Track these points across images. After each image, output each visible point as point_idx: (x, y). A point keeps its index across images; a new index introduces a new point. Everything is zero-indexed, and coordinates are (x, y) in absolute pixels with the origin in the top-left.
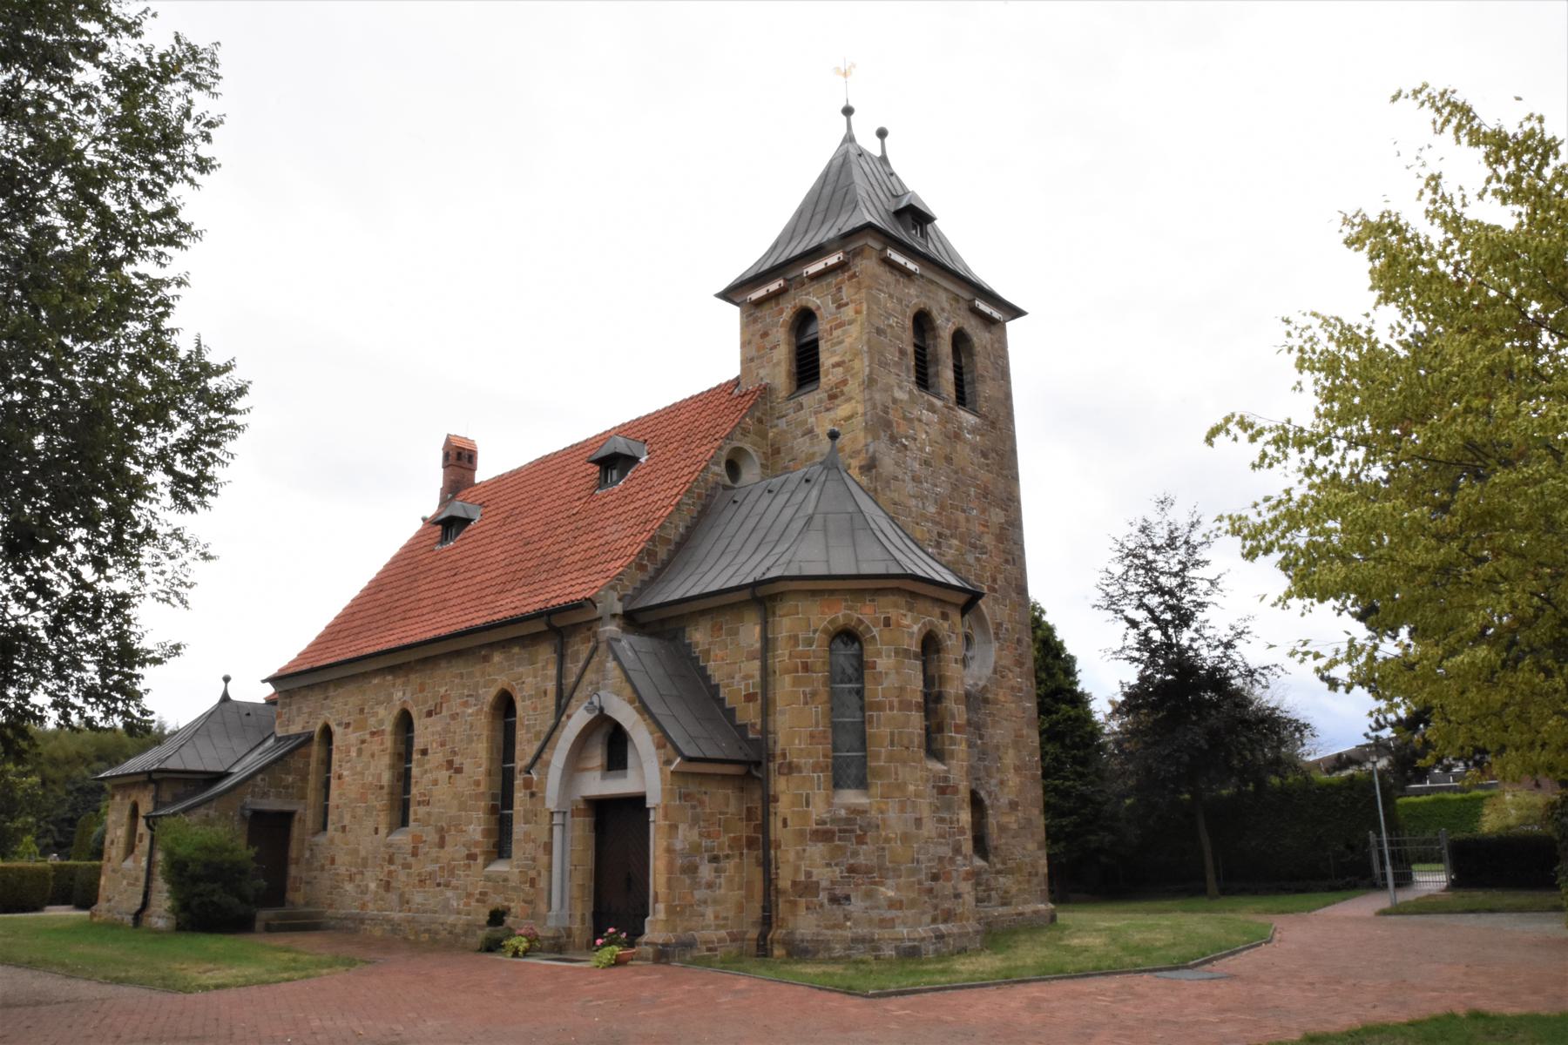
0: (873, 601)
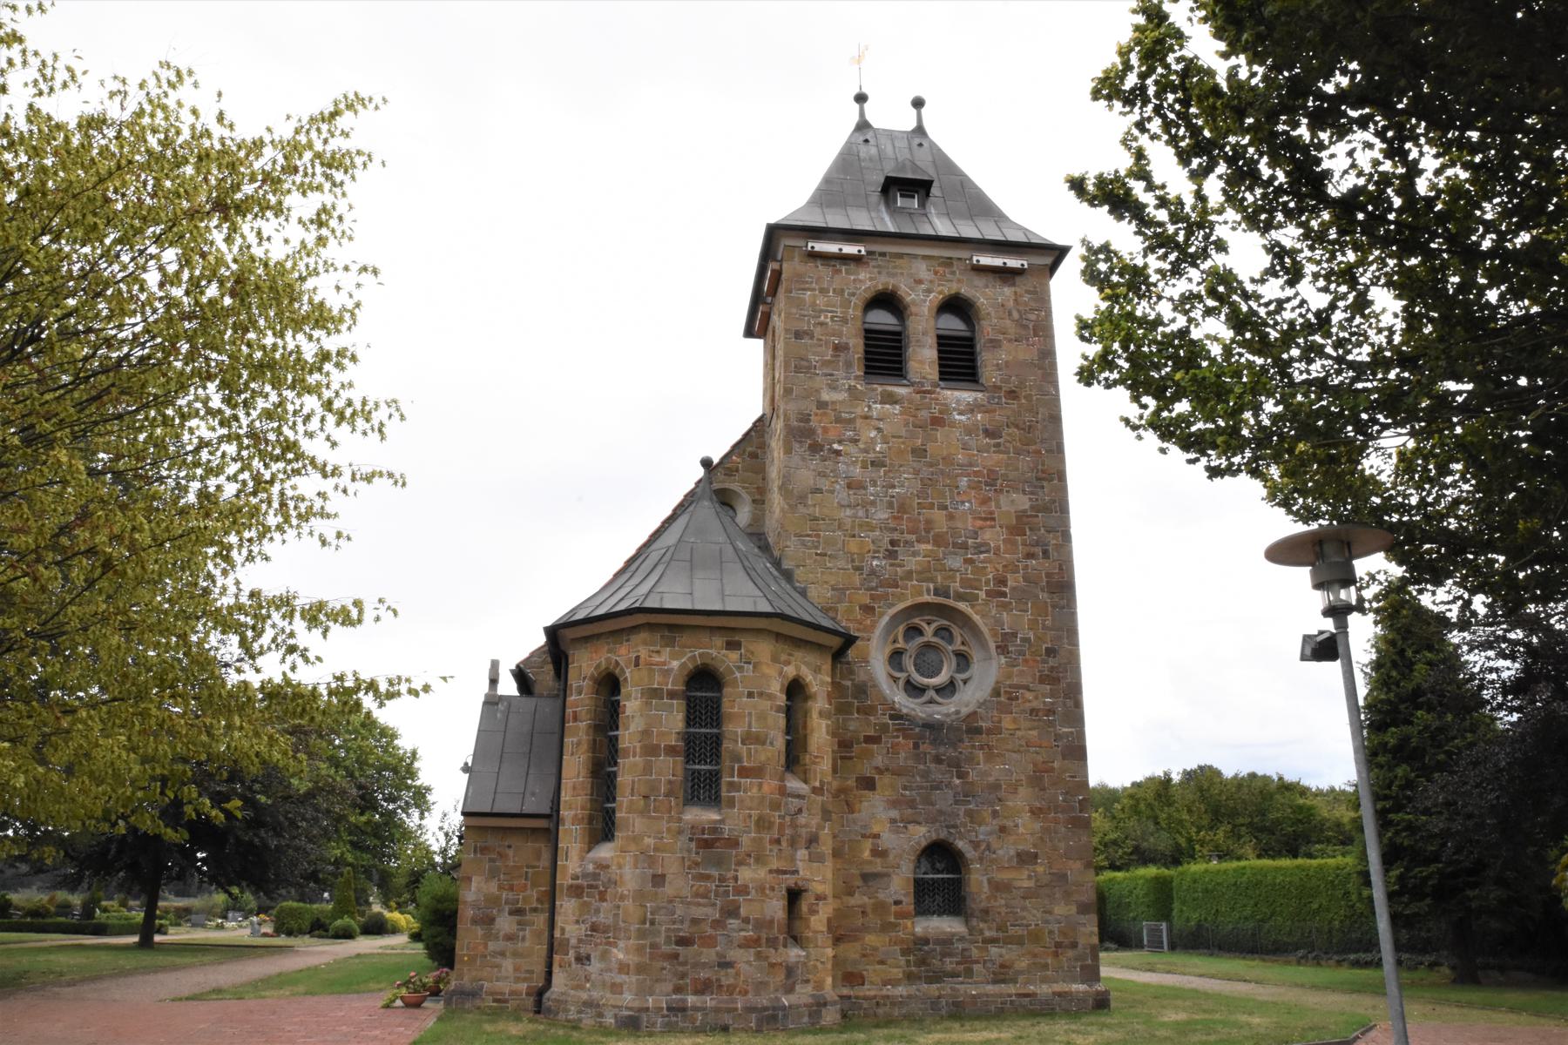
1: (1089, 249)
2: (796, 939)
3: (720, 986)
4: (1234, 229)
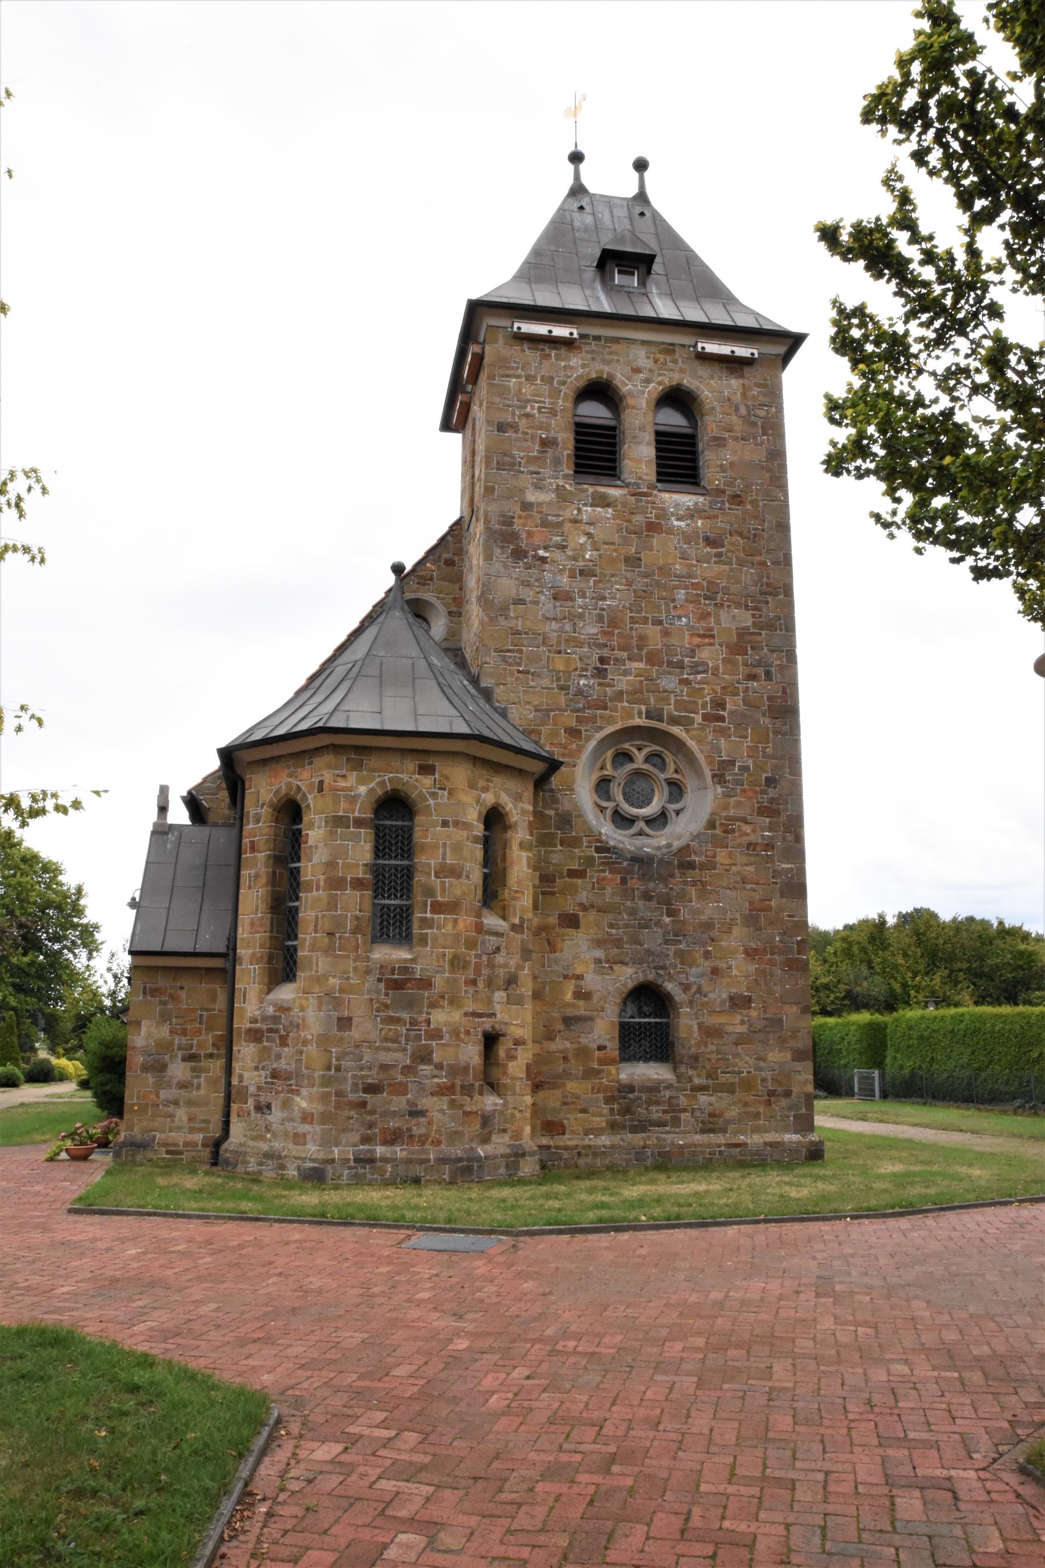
0: (310, 763)
1: (841, 311)
2: (493, 1086)
3: (411, 1137)
4: (1015, 291)
